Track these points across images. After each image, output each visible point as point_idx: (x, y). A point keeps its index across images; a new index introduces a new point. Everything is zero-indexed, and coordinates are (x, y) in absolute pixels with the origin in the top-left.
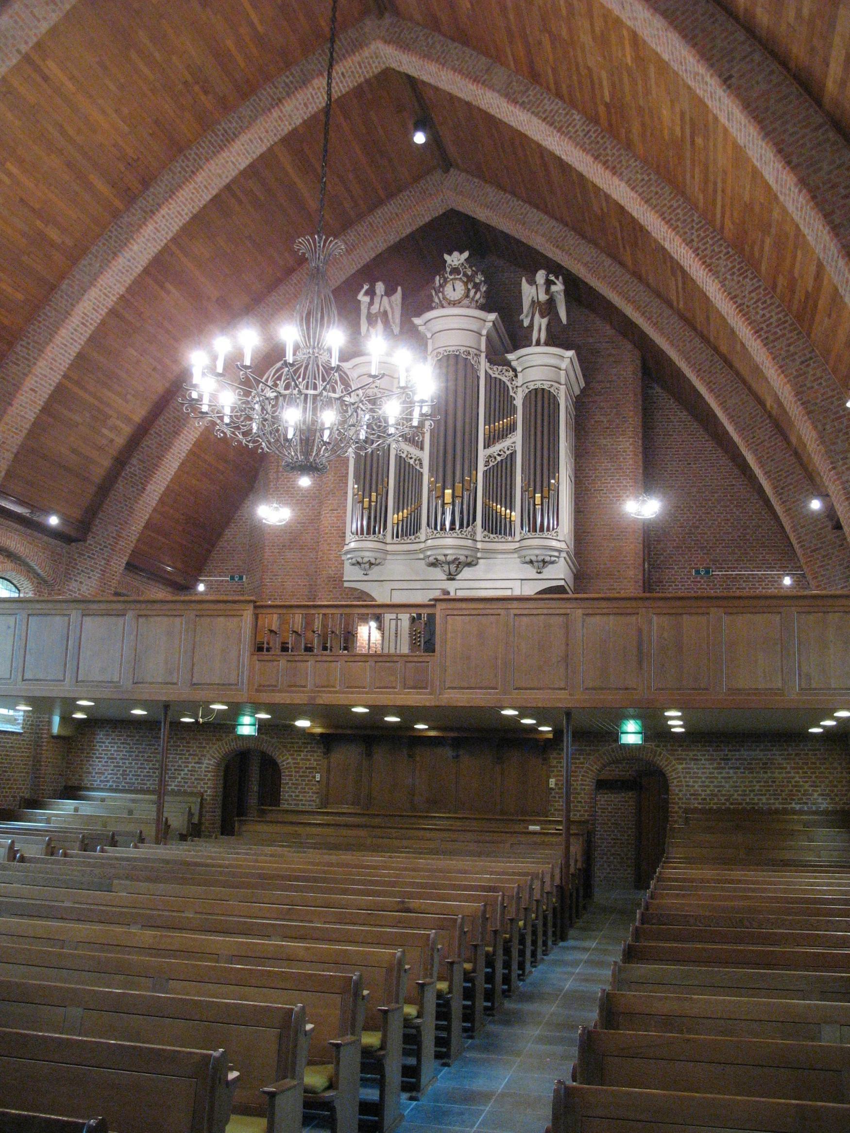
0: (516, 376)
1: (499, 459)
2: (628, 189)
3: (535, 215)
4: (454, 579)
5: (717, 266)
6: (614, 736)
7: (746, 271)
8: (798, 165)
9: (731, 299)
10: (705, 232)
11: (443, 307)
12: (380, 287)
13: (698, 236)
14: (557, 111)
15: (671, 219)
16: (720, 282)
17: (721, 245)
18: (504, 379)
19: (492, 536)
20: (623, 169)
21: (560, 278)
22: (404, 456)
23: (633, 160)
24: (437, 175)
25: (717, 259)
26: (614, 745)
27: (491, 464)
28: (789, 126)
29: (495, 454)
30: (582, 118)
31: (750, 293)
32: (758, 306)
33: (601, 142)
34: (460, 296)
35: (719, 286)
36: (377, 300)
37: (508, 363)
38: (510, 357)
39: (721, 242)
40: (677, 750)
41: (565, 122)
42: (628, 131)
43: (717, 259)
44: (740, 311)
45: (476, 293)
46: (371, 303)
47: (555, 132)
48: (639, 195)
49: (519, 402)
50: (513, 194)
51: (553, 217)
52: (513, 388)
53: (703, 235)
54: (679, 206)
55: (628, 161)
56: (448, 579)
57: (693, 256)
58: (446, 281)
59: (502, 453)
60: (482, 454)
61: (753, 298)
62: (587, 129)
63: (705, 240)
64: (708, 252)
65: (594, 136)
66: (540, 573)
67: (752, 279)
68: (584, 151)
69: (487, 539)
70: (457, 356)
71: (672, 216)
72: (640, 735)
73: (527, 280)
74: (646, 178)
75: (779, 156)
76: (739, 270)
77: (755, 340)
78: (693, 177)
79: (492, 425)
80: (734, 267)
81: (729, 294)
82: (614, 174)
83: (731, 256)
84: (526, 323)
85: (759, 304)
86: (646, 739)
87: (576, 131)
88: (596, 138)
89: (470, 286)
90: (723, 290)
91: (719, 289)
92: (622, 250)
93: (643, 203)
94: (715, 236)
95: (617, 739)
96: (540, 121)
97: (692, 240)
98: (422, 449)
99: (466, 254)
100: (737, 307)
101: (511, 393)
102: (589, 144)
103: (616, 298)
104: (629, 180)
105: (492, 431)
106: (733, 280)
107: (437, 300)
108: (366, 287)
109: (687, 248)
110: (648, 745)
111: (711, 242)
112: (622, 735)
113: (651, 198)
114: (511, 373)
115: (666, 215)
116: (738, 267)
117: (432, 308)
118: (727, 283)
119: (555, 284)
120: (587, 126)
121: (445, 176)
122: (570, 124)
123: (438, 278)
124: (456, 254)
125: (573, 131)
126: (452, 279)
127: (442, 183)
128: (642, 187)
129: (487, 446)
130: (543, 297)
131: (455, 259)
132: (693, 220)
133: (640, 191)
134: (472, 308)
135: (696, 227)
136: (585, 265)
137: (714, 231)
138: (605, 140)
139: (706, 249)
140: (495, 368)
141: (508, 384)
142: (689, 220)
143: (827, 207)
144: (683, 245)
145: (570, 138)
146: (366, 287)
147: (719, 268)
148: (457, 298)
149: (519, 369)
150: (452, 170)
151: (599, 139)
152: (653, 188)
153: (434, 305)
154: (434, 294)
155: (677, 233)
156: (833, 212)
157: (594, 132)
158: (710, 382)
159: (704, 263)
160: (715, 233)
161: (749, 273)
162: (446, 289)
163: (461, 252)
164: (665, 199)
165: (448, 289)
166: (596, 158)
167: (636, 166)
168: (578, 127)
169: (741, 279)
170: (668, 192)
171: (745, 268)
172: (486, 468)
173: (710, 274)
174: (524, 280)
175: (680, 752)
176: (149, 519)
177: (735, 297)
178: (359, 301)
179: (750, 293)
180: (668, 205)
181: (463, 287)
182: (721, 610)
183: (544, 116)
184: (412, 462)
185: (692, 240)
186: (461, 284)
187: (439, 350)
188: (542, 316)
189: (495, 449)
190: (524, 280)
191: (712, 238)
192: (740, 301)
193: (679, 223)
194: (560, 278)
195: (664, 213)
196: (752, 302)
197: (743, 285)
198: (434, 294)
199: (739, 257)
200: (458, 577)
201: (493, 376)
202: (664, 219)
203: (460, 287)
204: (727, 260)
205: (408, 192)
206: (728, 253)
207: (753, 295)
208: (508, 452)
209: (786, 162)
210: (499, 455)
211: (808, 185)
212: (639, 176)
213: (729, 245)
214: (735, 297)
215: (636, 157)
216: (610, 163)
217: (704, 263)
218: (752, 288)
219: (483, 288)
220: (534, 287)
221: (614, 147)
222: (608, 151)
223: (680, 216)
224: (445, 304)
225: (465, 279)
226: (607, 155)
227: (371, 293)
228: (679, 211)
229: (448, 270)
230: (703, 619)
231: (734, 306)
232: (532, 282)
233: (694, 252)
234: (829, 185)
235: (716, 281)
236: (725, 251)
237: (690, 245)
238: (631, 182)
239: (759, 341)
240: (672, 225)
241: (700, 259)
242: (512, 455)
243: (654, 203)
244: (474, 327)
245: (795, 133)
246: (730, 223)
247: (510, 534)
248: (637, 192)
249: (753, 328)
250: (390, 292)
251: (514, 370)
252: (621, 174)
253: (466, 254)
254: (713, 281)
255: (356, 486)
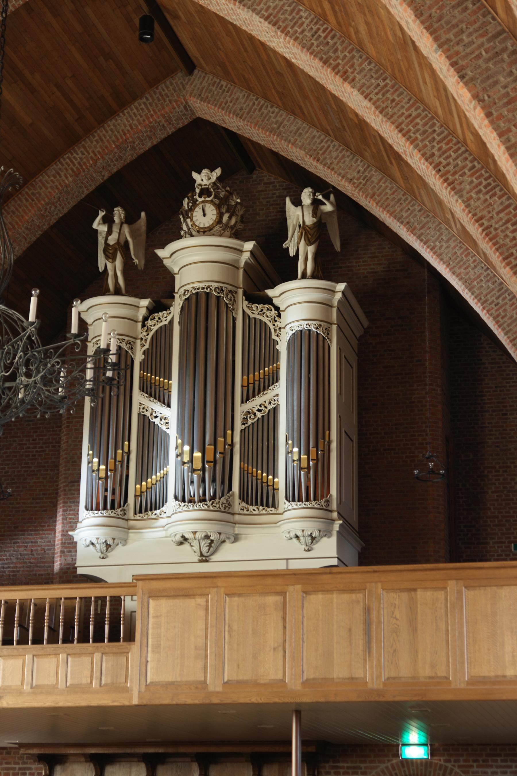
0: (279, 316)
1: (259, 415)
2: (361, 98)
3: (291, 123)
4: (206, 561)
5: (461, 183)
6: (394, 750)
7: (495, 187)
8: (472, 79)
9: (477, 221)
10: (447, 144)
11: (192, 236)
12: (119, 214)
13: (440, 149)
14: (281, 8)
15: (410, 130)
16: (464, 201)
17: (466, 159)
18: (265, 319)
19: (251, 508)
20: (355, 74)
21: (332, 197)
22: (148, 414)
23: (366, 63)
24: (179, 77)
25: (461, 176)
26: (395, 761)
27: (250, 422)
28: (464, 37)
29: (255, 410)
30: (310, 15)
31: (498, 213)
32: (507, 228)
33: (331, 42)
34: (211, 222)
35: (463, 206)
36: (116, 229)
37: (269, 301)
38: (270, 293)
39: (466, 155)
40: (472, 766)
41: (291, 21)
42: (357, 32)
43: (461, 176)
44: (487, 235)
45: (230, 218)
46: (110, 232)
47: (279, 33)
48: (374, 104)
49: (282, 348)
50: (266, 98)
51: (313, 124)
52: (275, 330)
53: (445, 147)
54: (419, 115)
55: (360, 65)
56: (201, 561)
57: (434, 172)
58: (195, 203)
59: (263, 408)
60: (240, 409)
61: (501, 219)
62: (315, 28)
63: (448, 154)
64: (451, 168)
65: (323, 35)
66: (308, 550)
67: (500, 197)
68: (311, 54)
69: (245, 512)
70: (207, 294)
71: (410, 127)
72: (426, 748)
73: (291, 200)
74: (382, 84)
75: (452, 70)
76: (485, 187)
77: (505, 268)
78: (425, 83)
79: (251, 376)
80: (480, 183)
81: (474, 215)
82: (345, 80)
83: (477, 171)
84: (292, 253)
85: (509, 225)
86: (433, 752)
87: (303, 31)
88: (325, 38)
89: (224, 210)
90: (467, 210)
91: (464, 210)
92: (388, 164)
93: (377, 112)
94: (459, 149)
95: (397, 754)
96: (262, 20)
97: (433, 155)
98: (169, 406)
99: (218, 172)
100: (483, 230)
101: (274, 337)
102: (317, 46)
103: (387, 219)
104: (362, 87)
105: (251, 381)
106: (479, 199)
107: (184, 227)
108: (102, 214)
109: (426, 163)
110: (436, 760)
111: (454, 155)
112: (403, 748)
113: (387, 107)
114: (274, 312)
115: (403, 126)
116: (484, 183)
117: (180, 237)
118: (472, 202)
119: (325, 204)
120: (316, 24)
121: (187, 79)
122: (295, 23)
123: (186, 201)
124: (205, 171)
125: (299, 30)
126: (202, 202)
127: (184, 88)
128: (377, 94)
129: (246, 399)
130: (309, 220)
131: (203, 178)
132: (434, 131)
133: (375, 98)
134: (226, 237)
135: (438, 138)
136: (350, 181)
137: (458, 142)
138: (335, 40)
139: (448, 164)
140: (254, 306)
141: (270, 325)
142: (430, 131)
143: (502, 125)
144: (423, 160)
145: (296, 39)
146: (102, 214)
147: (463, 186)
148: (207, 225)
149: (282, 308)
150: (196, 72)
151: (329, 39)
152: (388, 95)
153: (182, 233)
154: (182, 219)
155: (416, 147)
156: (509, 130)
157: (324, 31)
158: (498, 316)
159: (446, 180)
160: (460, 145)
161: (497, 190)
162: (195, 214)
163: (212, 170)
164: (403, 107)
165: (197, 213)
166: (325, 63)
167: (371, 70)
168: (305, 26)
169: (488, 197)
170: (406, 100)
171: (493, 184)
172: (243, 427)
173: (453, 193)
174: (288, 200)
175: (475, 769)
176: (55, 534)
177: (481, 218)
178: (96, 231)
179: (498, 213)
180: (407, 113)
181: (215, 212)
182: (461, 583)
183: (266, 14)
184: (157, 421)
185: (433, 155)
186: (212, 207)
187: (186, 288)
188: (309, 243)
189: (255, 403)
190: (288, 200)
191: (455, 151)
192: (486, 224)
193: (418, 135)
194: (332, 197)
195: (401, 124)
196: (501, 223)
197: (490, 204)
198: (182, 219)
199: (486, 172)
200: (214, 558)
201: (252, 316)
202: (400, 131)
203: (212, 211)
204: (472, 175)
205: (144, 100)
206: (474, 167)
207: (502, 215)
208: (270, 407)
209: (459, 77)
210: (259, 411)
211: (483, 101)
212: (373, 81)
213: (475, 159)
214: (481, 218)
215: (369, 59)
216: (340, 67)
217: (446, 180)
218: (501, 208)
219: (240, 212)
220: (300, 208)
221: (345, 49)
222: (339, 53)
223: (419, 127)
224: (194, 233)
225: (217, 201)
226: (338, 57)
227: (108, 220)
228: (418, 120)
229: (198, 191)
230: (441, 595)
231: (480, 229)
232: (297, 202)
233: (434, 168)
234: (505, 100)
235: (460, 201)
236: (470, 165)
237: (430, 160)
238: (364, 89)
239: (508, 268)
240: (410, 137)
241: (441, 176)
242: (275, 410)
243: (390, 113)
244: (228, 256)
245: (472, 42)
246: (470, 135)
247: (273, 506)
248: (370, 100)
249: (501, 254)
250: (130, 219)
251: (277, 309)
252: (353, 80)
253: (218, 172)
254: (457, 201)
255: (91, 452)
